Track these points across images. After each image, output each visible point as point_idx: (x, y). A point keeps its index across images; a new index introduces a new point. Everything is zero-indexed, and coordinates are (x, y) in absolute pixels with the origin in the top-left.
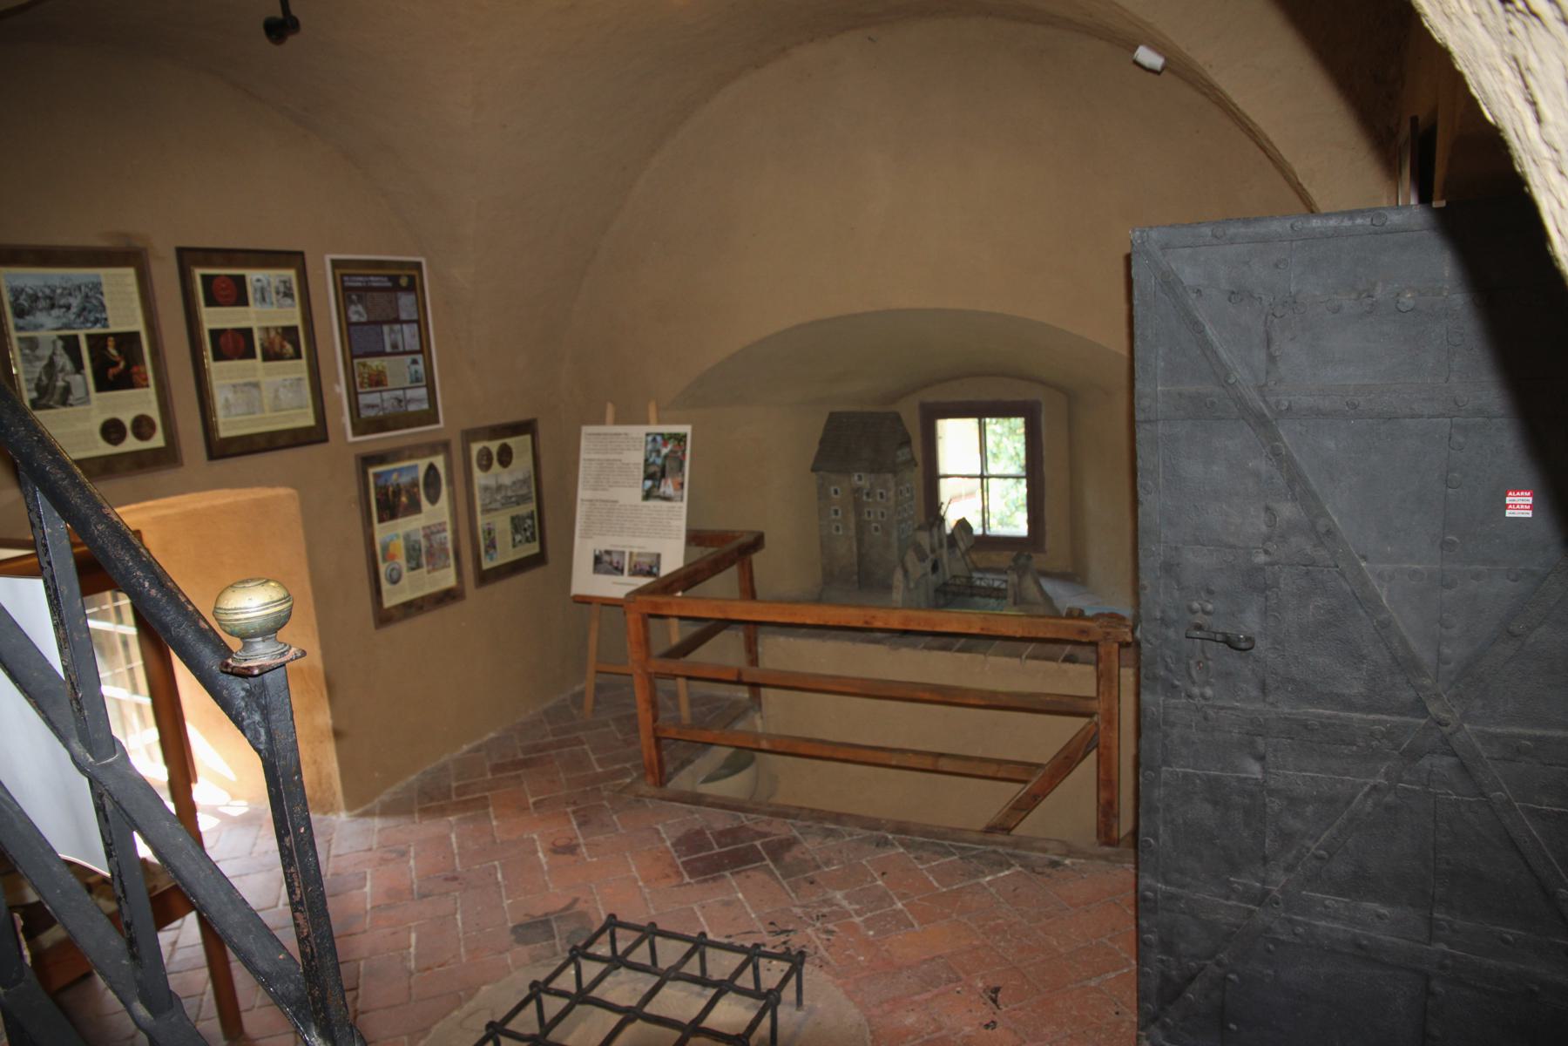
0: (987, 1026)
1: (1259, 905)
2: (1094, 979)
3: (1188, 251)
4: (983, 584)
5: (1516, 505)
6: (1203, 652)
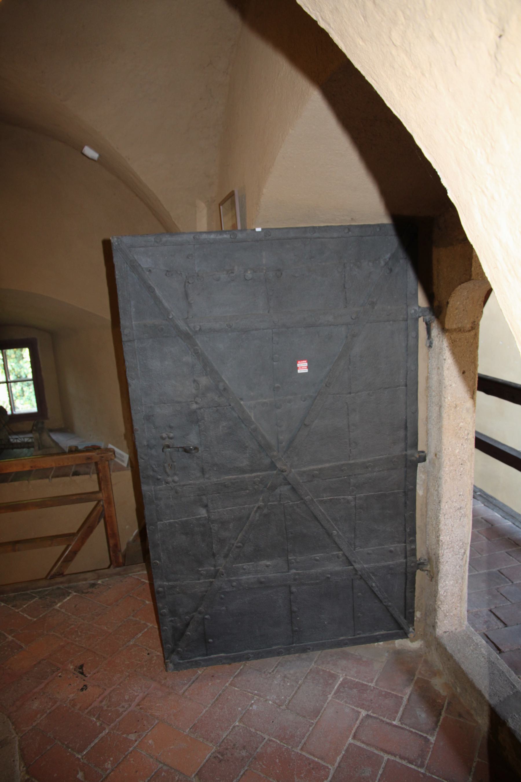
0: (82, 689)
1: (214, 578)
2: (131, 640)
3: (142, 249)
4: (18, 441)
5: (301, 367)
6: (171, 459)
